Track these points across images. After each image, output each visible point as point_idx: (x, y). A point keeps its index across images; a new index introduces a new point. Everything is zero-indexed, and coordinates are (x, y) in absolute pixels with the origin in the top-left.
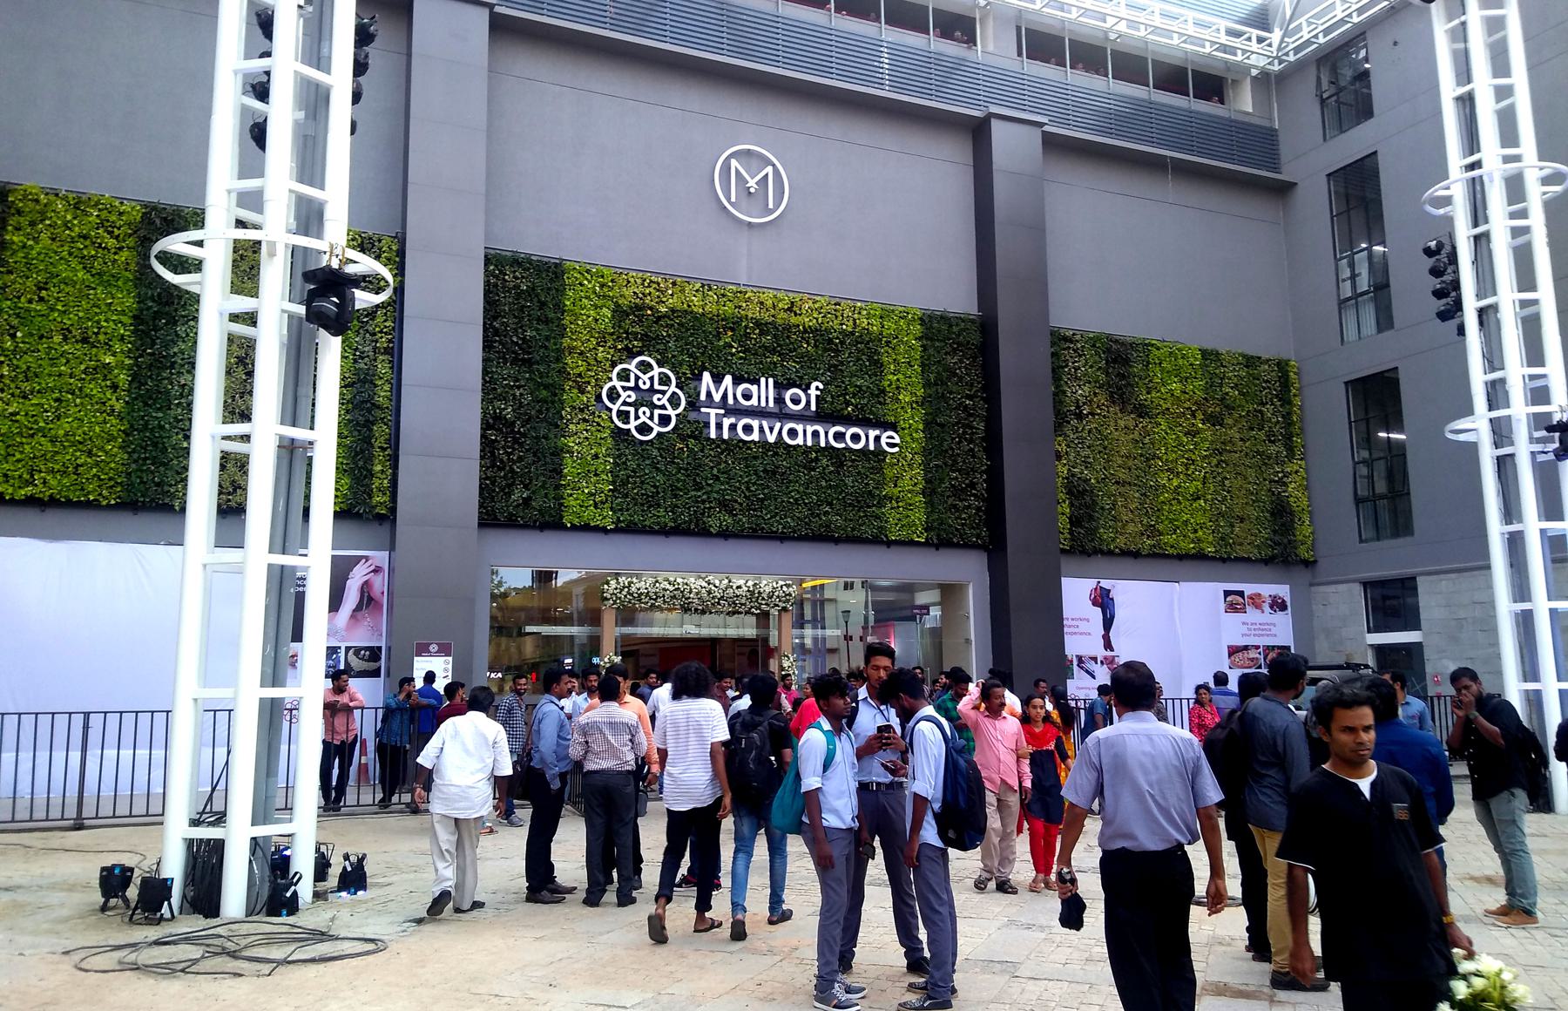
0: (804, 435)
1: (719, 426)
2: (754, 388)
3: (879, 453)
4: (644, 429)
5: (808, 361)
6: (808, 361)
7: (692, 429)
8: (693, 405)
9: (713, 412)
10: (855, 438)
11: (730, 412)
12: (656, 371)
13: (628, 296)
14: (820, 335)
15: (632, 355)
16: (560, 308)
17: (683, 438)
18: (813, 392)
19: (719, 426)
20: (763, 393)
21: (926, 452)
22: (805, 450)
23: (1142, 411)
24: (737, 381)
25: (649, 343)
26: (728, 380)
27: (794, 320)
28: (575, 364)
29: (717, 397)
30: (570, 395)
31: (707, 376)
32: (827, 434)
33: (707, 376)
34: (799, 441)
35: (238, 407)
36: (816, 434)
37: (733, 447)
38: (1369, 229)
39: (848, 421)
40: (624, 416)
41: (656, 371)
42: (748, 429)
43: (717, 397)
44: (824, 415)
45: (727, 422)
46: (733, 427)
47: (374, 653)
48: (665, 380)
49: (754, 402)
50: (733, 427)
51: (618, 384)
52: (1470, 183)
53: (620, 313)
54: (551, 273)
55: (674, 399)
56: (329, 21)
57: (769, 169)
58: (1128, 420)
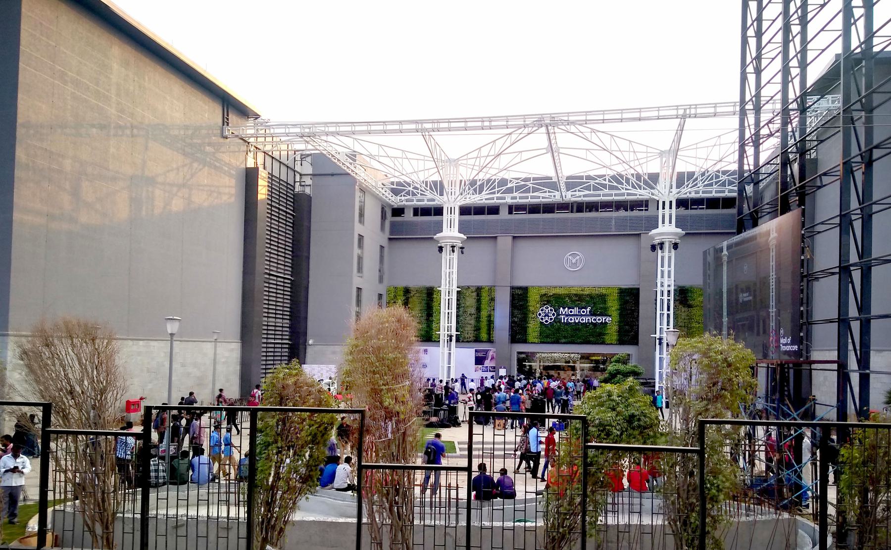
0: (585, 320)
1: (564, 319)
2: (573, 310)
3: (606, 323)
4: (546, 321)
5: (588, 302)
6: (588, 302)
7: (557, 320)
8: (558, 315)
9: (563, 316)
10: (599, 319)
11: (567, 316)
12: (550, 308)
13: (543, 292)
14: (591, 296)
15: (545, 305)
16: (527, 297)
17: (556, 322)
18: (588, 310)
19: (564, 319)
20: (575, 311)
21: (620, 322)
22: (585, 323)
23: (690, 306)
24: (569, 308)
25: (548, 302)
26: (567, 308)
27: (584, 293)
28: (531, 309)
29: (564, 313)
30: (531, 315)
31: (561, 308)
32: (592, 319)
33: (561, 308)
34: (584, 321)
35: (662, 266)
36: (588, 319)
37: (568, 324)
38: (753, 254)
39: (599, 315)
40: (542, 319)
41: (550, 308)
42: (571, 319)
43: (564, 313)
44: (592, 314)
45: (566, 318)
46: (567, 319)
47: (494, 368)
48: (551, 310)
49: (573, 313)
50: (567, 319)
51: (541, 312)
52: (394, 242)
53: (542, 296)
54: (525, 290)
55: (554, 315)
56: (261, 265)
57: (578, 257)
58: (686, 309)
